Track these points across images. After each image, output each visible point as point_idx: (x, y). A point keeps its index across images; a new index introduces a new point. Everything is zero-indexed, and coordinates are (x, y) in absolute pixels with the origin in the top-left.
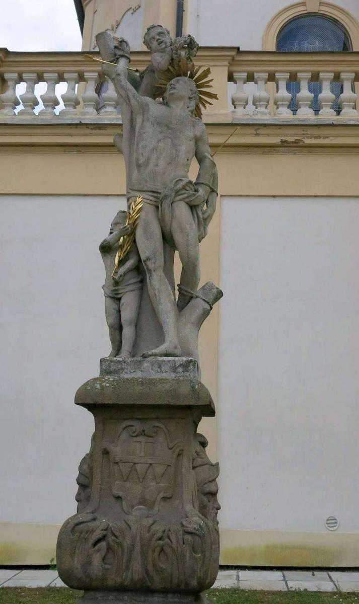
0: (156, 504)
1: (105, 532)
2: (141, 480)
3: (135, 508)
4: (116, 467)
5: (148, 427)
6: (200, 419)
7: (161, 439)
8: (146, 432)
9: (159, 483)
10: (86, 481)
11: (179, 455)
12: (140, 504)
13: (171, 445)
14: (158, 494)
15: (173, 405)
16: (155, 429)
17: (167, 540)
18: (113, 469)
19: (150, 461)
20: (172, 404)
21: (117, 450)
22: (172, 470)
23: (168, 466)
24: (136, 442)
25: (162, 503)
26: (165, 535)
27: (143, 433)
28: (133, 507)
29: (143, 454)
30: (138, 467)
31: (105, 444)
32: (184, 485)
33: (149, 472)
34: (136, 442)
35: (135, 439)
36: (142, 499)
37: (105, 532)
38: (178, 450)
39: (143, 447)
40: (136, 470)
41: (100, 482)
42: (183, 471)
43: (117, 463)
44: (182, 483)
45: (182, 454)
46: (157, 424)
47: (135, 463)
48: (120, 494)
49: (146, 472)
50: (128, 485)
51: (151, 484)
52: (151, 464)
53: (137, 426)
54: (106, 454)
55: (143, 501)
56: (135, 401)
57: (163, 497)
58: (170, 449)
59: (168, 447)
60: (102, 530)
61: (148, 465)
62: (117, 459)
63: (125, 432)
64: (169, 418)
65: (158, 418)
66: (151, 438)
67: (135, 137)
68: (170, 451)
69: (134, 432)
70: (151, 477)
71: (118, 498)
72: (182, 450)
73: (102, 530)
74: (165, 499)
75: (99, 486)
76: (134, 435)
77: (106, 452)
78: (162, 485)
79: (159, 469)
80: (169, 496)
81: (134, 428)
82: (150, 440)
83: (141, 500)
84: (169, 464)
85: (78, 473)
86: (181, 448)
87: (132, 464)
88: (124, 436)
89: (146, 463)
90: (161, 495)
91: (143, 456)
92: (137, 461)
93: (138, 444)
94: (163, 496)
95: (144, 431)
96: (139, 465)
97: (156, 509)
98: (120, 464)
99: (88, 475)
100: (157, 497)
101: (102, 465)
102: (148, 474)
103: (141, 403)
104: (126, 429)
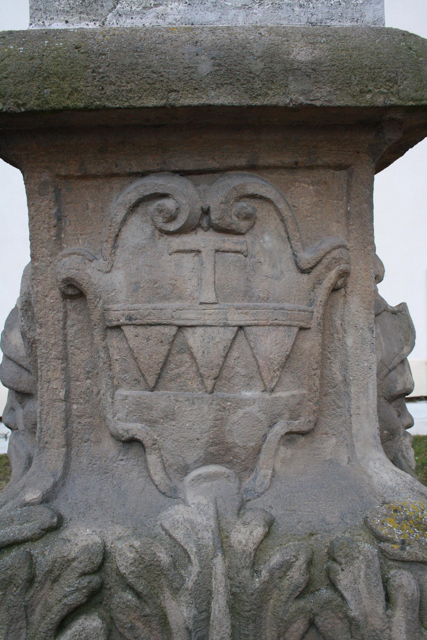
0: (262, 456)
1: (96, 579)
2: (209, 383)
3: (194, 474)
4: (114, 341)
5: (217, 195)
6: (373, 180)
7: (267, 240)
8: (214, 216)
9: (272, 391)
10: (25, 382)
11: (335, 289)
12: (208, 460)
13: (307, 257)
14: (271, 426)
15: (322, 108)
16: (246, 206)
17: (325, 593)
18: (106, 349)
19: (236, 318)
20: (318, 103)
21: (114, 283)
22: (311, 343)
23: (302, 329)
24: (178, 252)
25: (285, 452)
26: (318, 573)
27: (202, 221)
28: (185, 470)
29: (209, 295)
30: (194, 339)
31: (68, 265)
32: (353, 389)
33: (235, 354)
34: (178, 252)
35: (177, 242)
36: (213, 444)
37: (96, 579)
38: (333, 274)
39: (209, 266)
40: (189, 350)
41: (62, 394)
42: (349, 341)
43: (118, 327)
44: (346, 381)
45: (345, 285)
46: (255, 184)
47: (180, 327)
48: (136, 429)
49: (226, 357)
50: (162, 399)
51: (248, 394)
52: (241, 327)
53: (184, 195)
54: (72, 297)
55: (219, 452)
56: (173, 95)
57: (287, 434)
58: (303, 271)
59: (296, 263)
60: (84, 574)
61: (230, 334)
62: (117, 314)
63: (135, 220)
64: (294, 167)
65: (252, 168)
66: (235, 238)
67: (66, 31)
68: (305, 277)
69: (172, 218)
70: (243, 372)
71: (131, 442)
72: (344, 274)
73: (84, 574)
74: (291, 437)
75: (62, 405)
76: (172, 227)
77: (74, 292)
78: (282, 394)
79: (271, 344)
80: (305, 428)
81: (169, 204)
82: (229, 242)
83: (211, 449)
84: (302, 324)
85: (376, 242)
86: (343, 266)
87: (175, 329)
88: (137, 231)
89: (226, 326)
90: (280, 428)
91: (213, 300)
92: (190, 316)
93: (188, 261)
94: (286, 430)
95: (206, 212)
96: (199, 331)
97: (264, 472)
98: (129, 331)
99: (25, 363)
100: (265, 436)
101: (65, 335)
102: (231, 361)
103: (196, 102)
104: (140, 210)
